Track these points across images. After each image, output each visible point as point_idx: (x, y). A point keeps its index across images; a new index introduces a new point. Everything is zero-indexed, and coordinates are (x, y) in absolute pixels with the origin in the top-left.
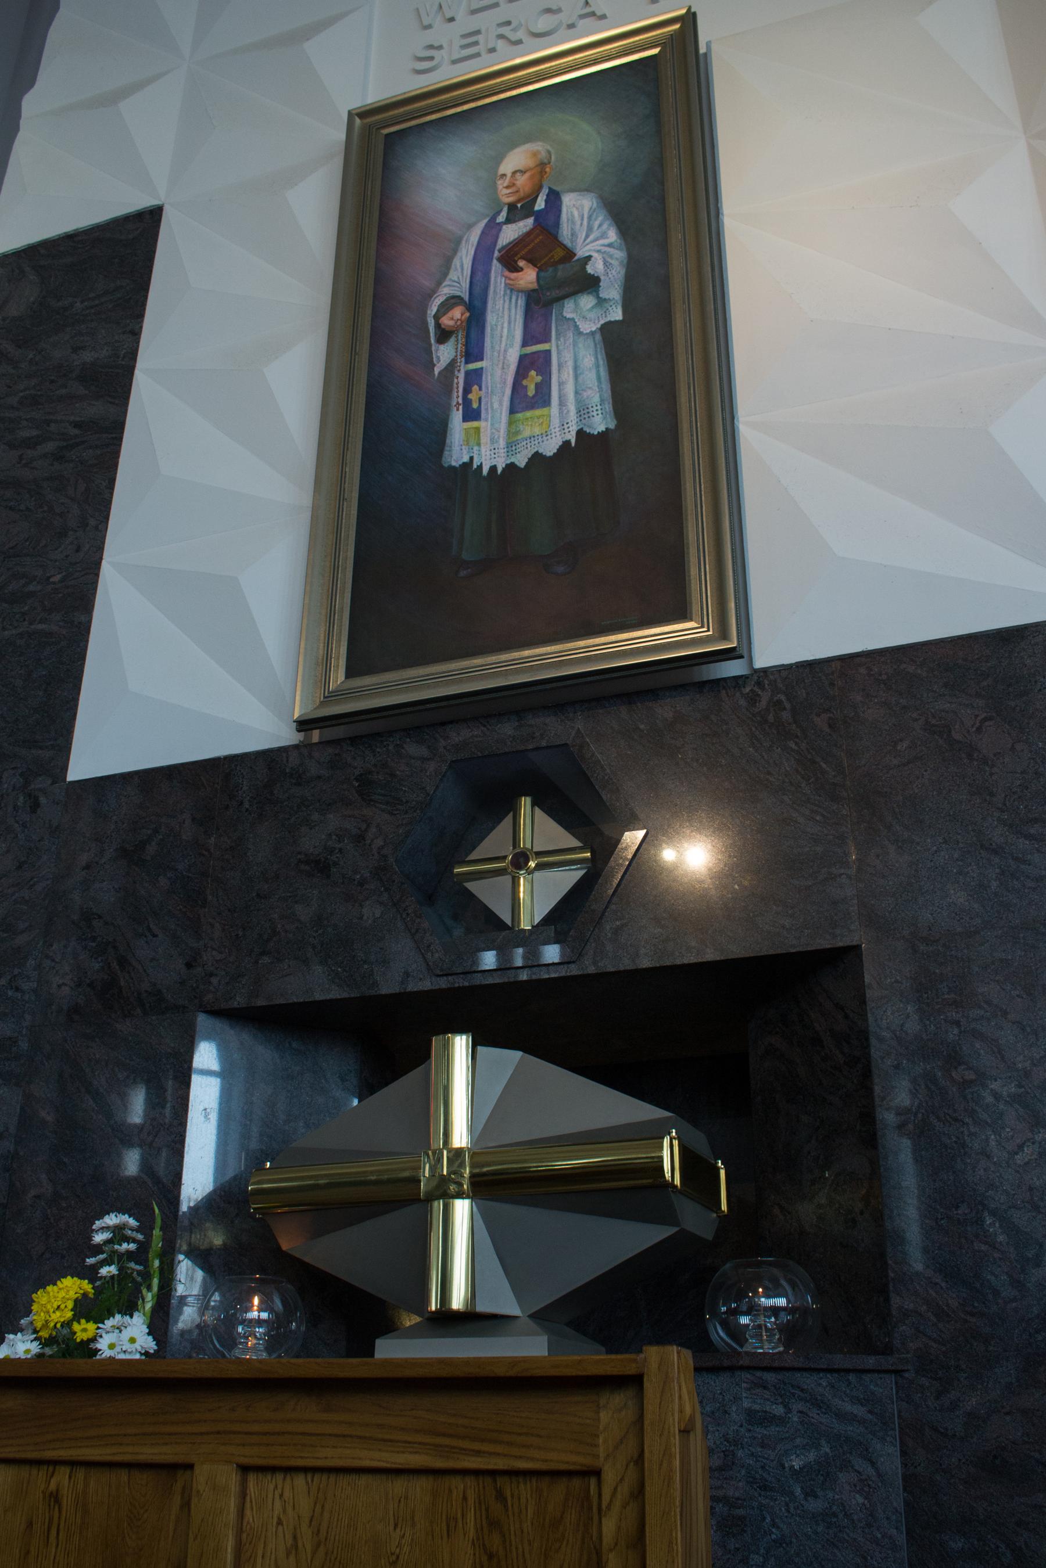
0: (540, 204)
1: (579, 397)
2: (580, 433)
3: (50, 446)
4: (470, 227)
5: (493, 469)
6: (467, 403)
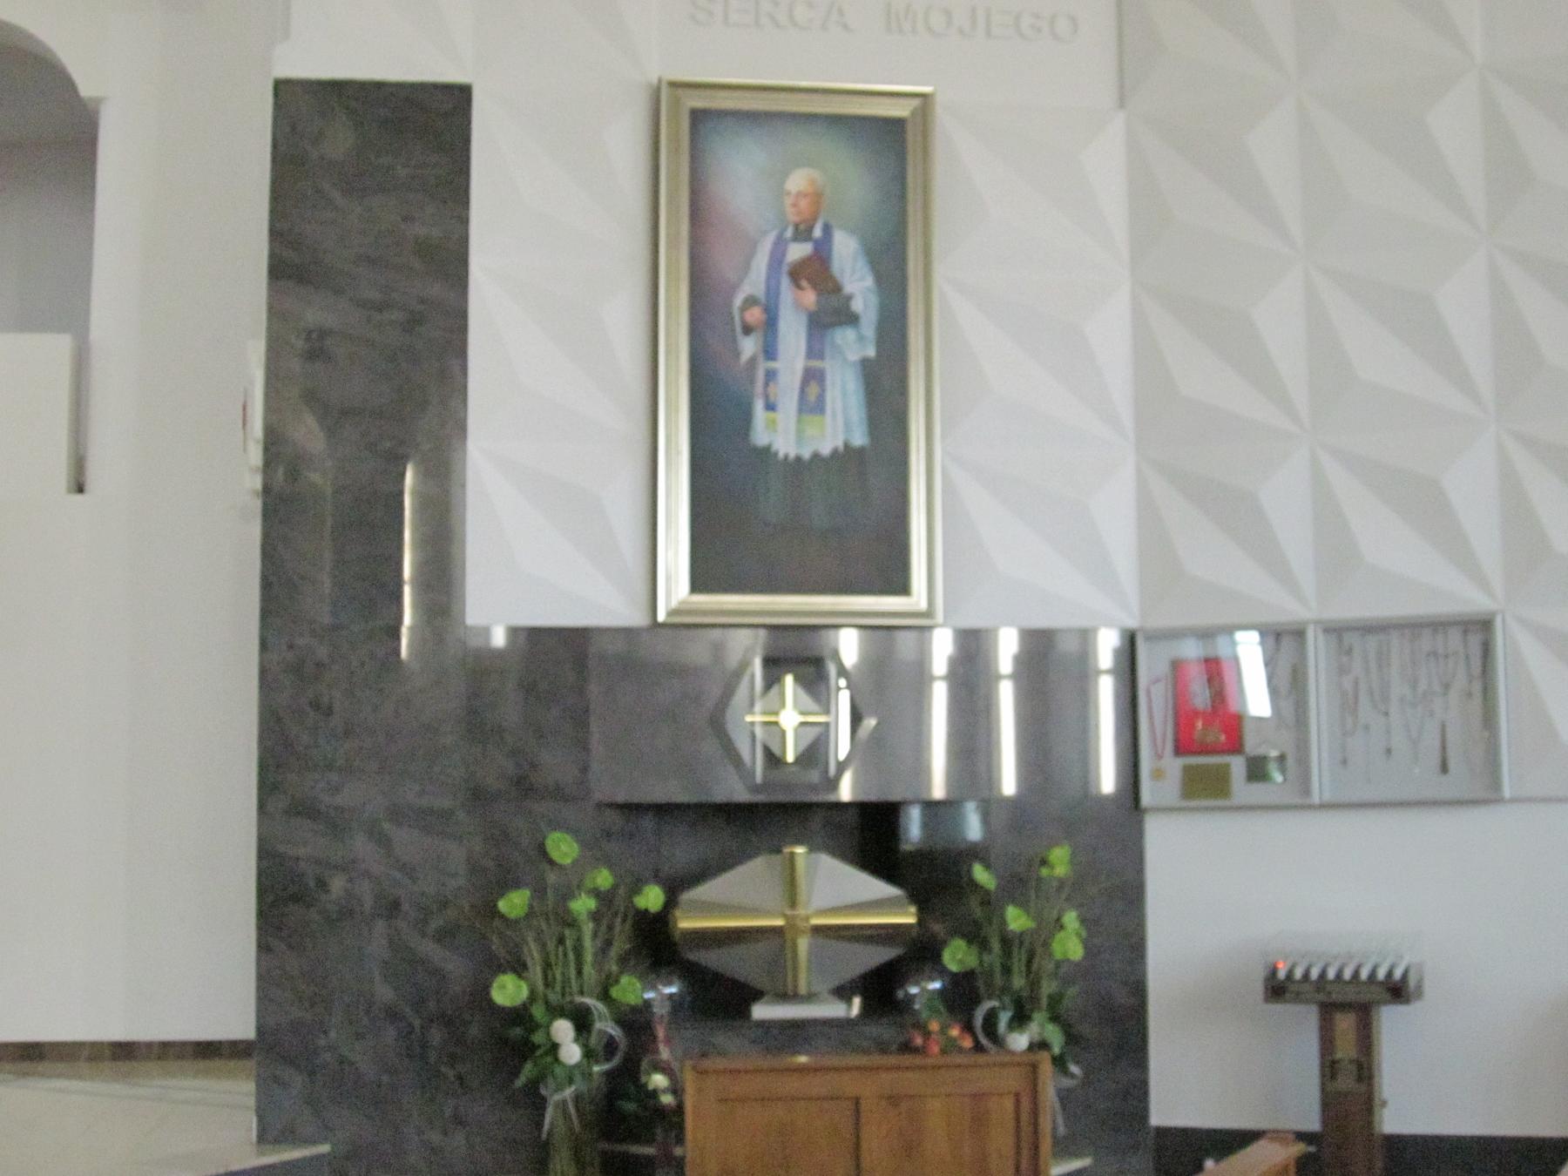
1: (841, 424)
2: (846, 445)
3: (396, 315)
4: (765, 233)
5: (786, 457)
6: (767, 397)
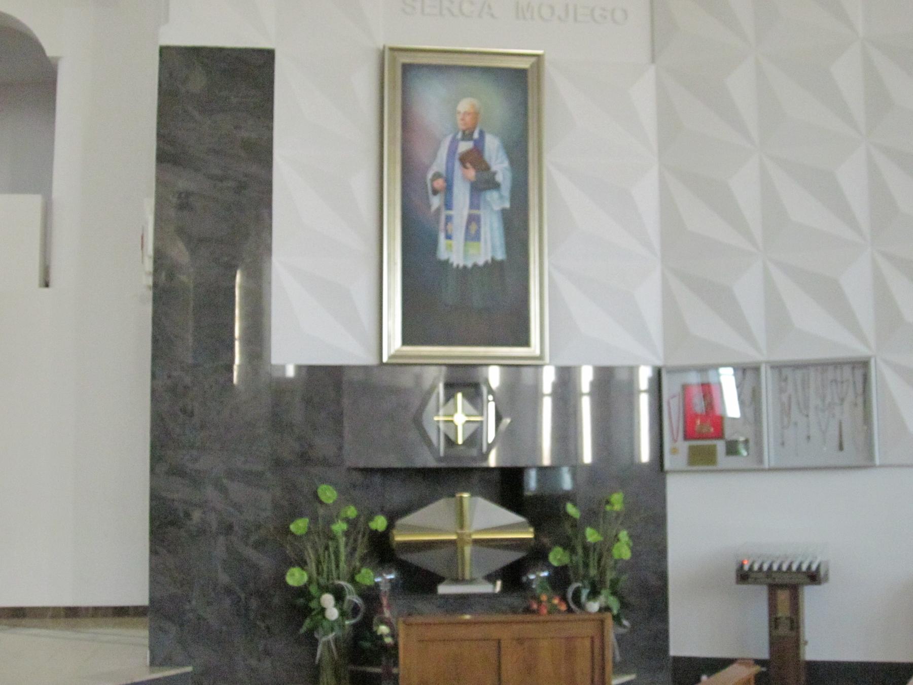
0: (476, 135)
1: (490, 247)
2: (493, 259)
3: (230, 184)
4: (445, 136)
5: (458, 266)
6: (446, 231)
